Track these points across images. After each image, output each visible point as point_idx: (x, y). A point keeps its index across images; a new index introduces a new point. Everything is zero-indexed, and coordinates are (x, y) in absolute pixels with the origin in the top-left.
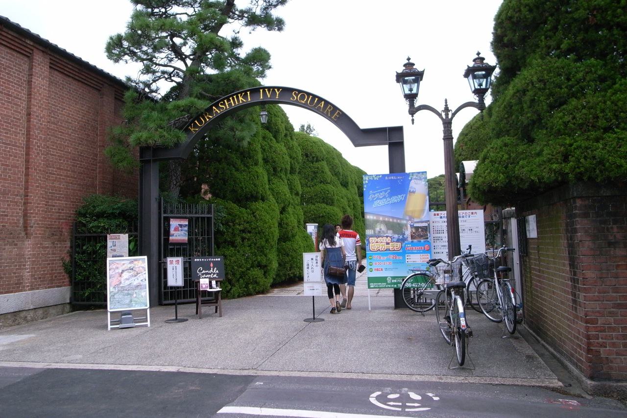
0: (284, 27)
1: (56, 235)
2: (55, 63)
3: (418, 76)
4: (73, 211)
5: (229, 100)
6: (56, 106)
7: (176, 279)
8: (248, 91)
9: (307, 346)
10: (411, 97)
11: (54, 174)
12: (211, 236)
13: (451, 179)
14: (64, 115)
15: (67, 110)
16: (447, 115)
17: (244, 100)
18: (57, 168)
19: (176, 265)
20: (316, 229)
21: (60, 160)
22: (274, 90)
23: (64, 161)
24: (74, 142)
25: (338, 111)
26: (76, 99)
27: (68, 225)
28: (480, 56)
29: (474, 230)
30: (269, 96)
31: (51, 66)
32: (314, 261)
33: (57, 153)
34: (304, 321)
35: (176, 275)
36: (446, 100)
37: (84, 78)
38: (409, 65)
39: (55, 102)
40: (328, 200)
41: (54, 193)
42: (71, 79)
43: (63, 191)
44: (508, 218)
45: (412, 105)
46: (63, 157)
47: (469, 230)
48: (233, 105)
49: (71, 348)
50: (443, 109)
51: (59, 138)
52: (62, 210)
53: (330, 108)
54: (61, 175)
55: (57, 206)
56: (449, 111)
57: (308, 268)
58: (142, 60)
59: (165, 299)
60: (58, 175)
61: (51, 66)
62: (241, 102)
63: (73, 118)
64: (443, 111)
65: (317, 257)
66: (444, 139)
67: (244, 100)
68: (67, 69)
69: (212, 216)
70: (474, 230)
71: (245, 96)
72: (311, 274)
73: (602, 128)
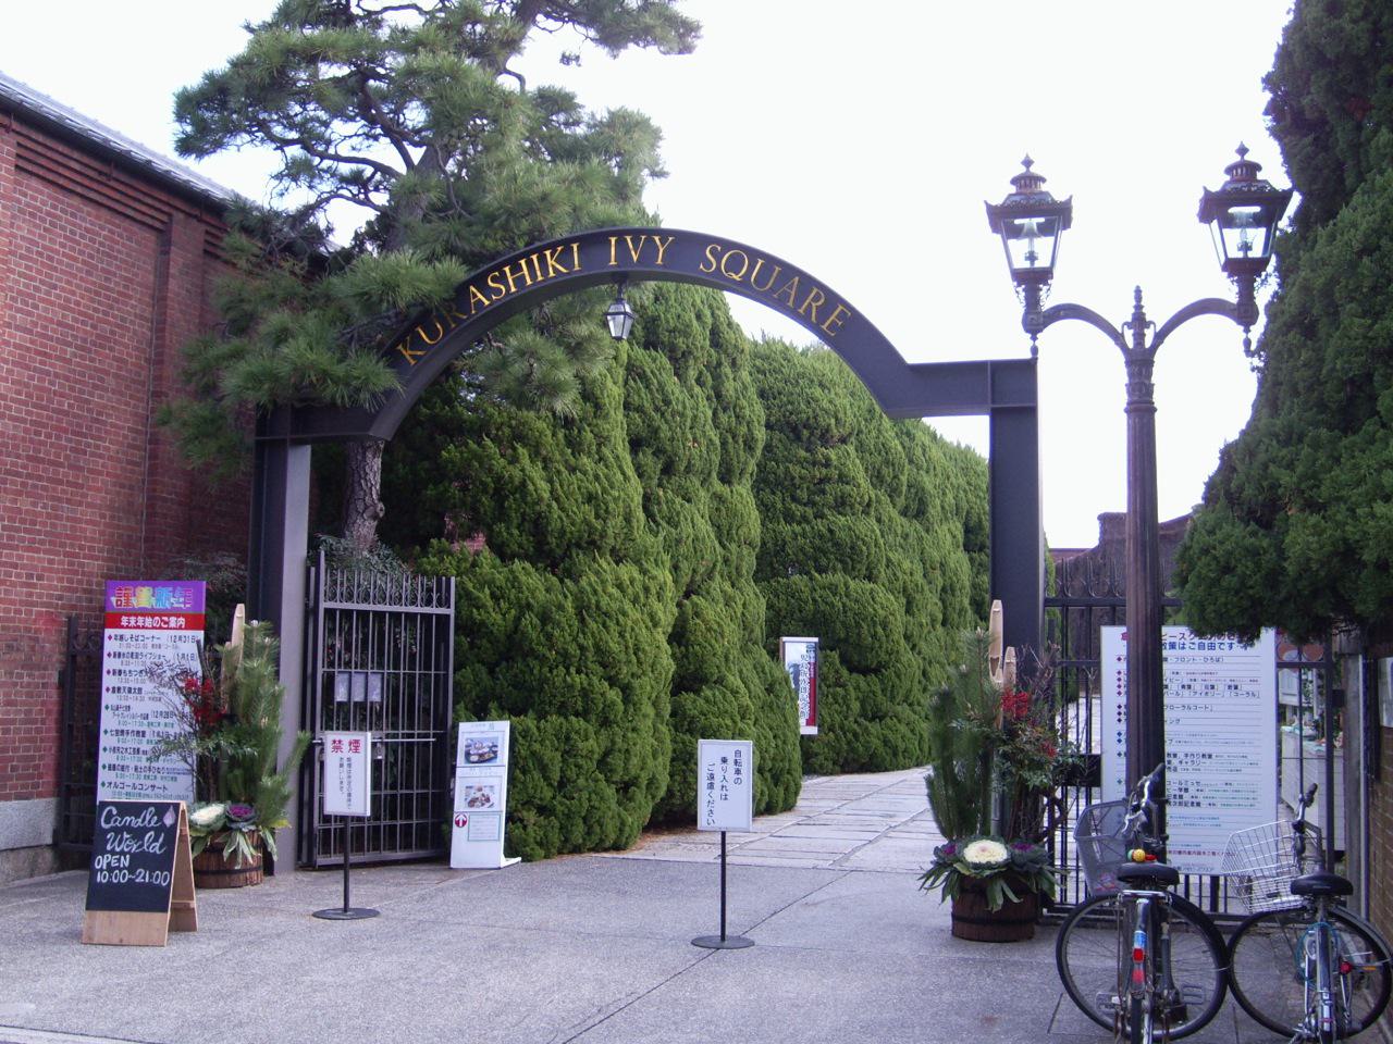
0: (697, 42)
1: (18, 650)
2: (31, 156)
3: (1057, 216)
4: (61, 580)
5: (516, 268)
6: (32, 279)
7: (349, 795)
8: (574, 240)
9: (675, 1023)
10: (1032, 280)
11: (18, 474)
12: (447, 669)
13: (1143, 534)
14: (52, 303)
15: (63, 289)
16: (1139, 337)
17: (419, 353)
18: (29, 458)
19: (351, 755)
20: (812, 654)
21: (38, 433)
22: (650, 241)
23: (49, 436)
24: (80, 382)
25: (841, 308)
26: (91, 256)
27: (53, 620)
28: (1248, 157)
29: (1245, 688)
30: (635, 258)
31: (22, 163)
32: (731, 766)
33: (28, 413)
34: (694, 943)
35: (349, 783)
36: (1138, 292)
37: (117, 196)
38: (1027, 180)
39: (27, 267)
40: (850, 557)
41: (18, 530)
42: (76, 201)
43: (44, 524)
44: (1350, 655)
45: (1032, 301)
46: (45, 426)
47: (1230, 687)
48: (529, 282)
49: (14, 981)
50: (1129, 319)
51: (35, 369)
52: (40, 578)
53: (816, 298)
54: (40, 478)
55: (24, 567)
56: (1147, 324)
57: (711, 786)
58: (283, 144)
59: (326, 852)
60: (29, 476)
61: (22, 163)
62: (552, 274)
63: (80, 313)
64: (1125, 324)
65: (738, 753)
66: (1127, 411)
67: (419, 353)
68: (67, 173)
69: (451, 611)
70: (1245, 688)
71: (565, 258)
72: (719, 805)
73: (539, 722)
